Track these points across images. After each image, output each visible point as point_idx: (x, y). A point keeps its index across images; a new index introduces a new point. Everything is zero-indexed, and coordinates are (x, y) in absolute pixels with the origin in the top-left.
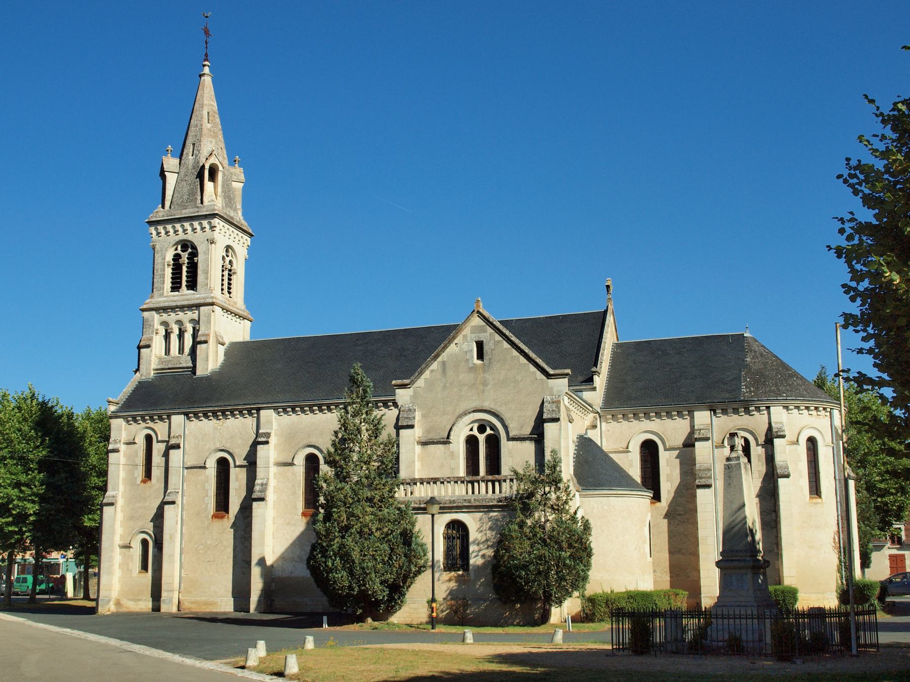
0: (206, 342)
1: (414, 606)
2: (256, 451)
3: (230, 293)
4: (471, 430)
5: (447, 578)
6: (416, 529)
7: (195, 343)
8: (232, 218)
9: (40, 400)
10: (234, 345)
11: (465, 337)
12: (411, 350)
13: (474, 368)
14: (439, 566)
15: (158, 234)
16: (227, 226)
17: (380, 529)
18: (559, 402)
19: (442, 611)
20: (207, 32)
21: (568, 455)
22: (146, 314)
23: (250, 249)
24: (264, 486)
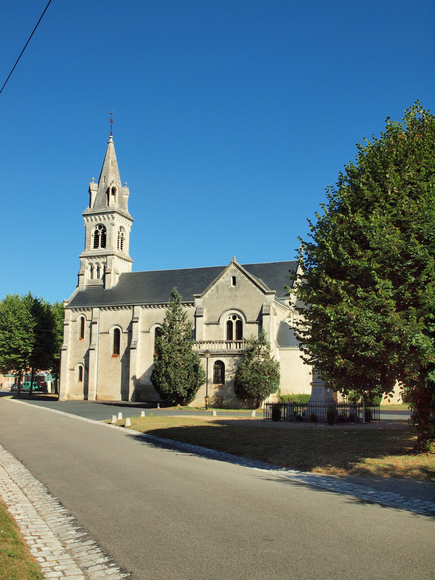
0: (110, 273)
1: (199, 400)
2: (132, 326)
3: (122, 249)
4: (229, 318)
5: (214, 387)
6: (201, 364)
7: (105, 274)
8: (123, 213)
9: (34, 299)
10: (123, 274)
11: (227, 274)
12: (201, 279)
13: (231, 289)
14: (211, 381)
15: (88, 220)
16: (120, 217)
17: (184, 364)
18: (270, 306)
19: (212, 402)
20: (111, 121)
21: (273, 331)
22: (82, 259)
23: (132, 228)
24: (136, 342)
